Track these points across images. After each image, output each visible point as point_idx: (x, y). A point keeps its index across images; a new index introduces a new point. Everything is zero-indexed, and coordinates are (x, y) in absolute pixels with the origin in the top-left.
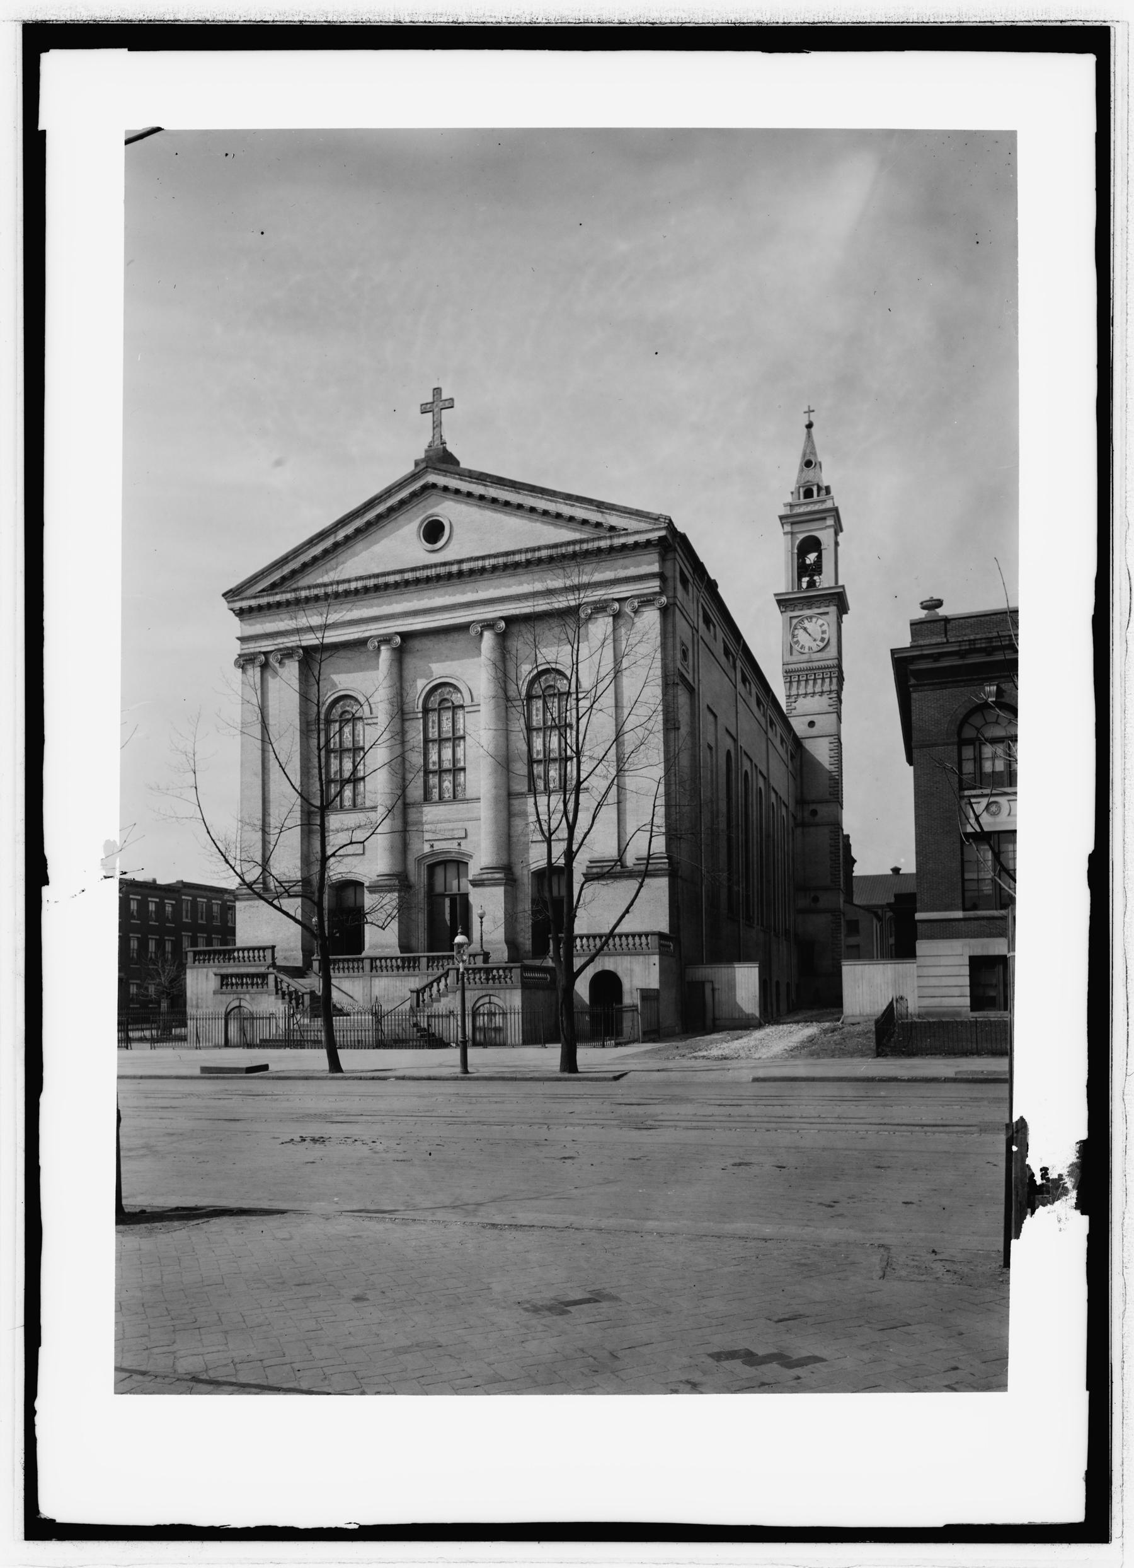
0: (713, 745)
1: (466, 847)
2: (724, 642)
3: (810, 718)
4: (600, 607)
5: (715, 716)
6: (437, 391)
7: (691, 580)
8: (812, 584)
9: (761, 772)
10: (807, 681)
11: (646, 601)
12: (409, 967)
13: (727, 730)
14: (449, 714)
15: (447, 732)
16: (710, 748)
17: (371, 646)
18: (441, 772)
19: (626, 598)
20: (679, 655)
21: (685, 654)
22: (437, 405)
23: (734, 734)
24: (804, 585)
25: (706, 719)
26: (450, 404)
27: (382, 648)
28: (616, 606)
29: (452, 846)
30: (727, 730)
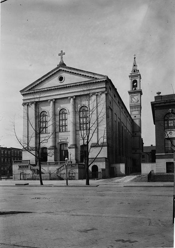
3: (135, 116)
4: (94, 94)
6: (62, 51)
8: (135, 89)
11: (103, 92)
19: (99, 92)
21: (110, 103)
22: (62, 54)
29: (65, 140)
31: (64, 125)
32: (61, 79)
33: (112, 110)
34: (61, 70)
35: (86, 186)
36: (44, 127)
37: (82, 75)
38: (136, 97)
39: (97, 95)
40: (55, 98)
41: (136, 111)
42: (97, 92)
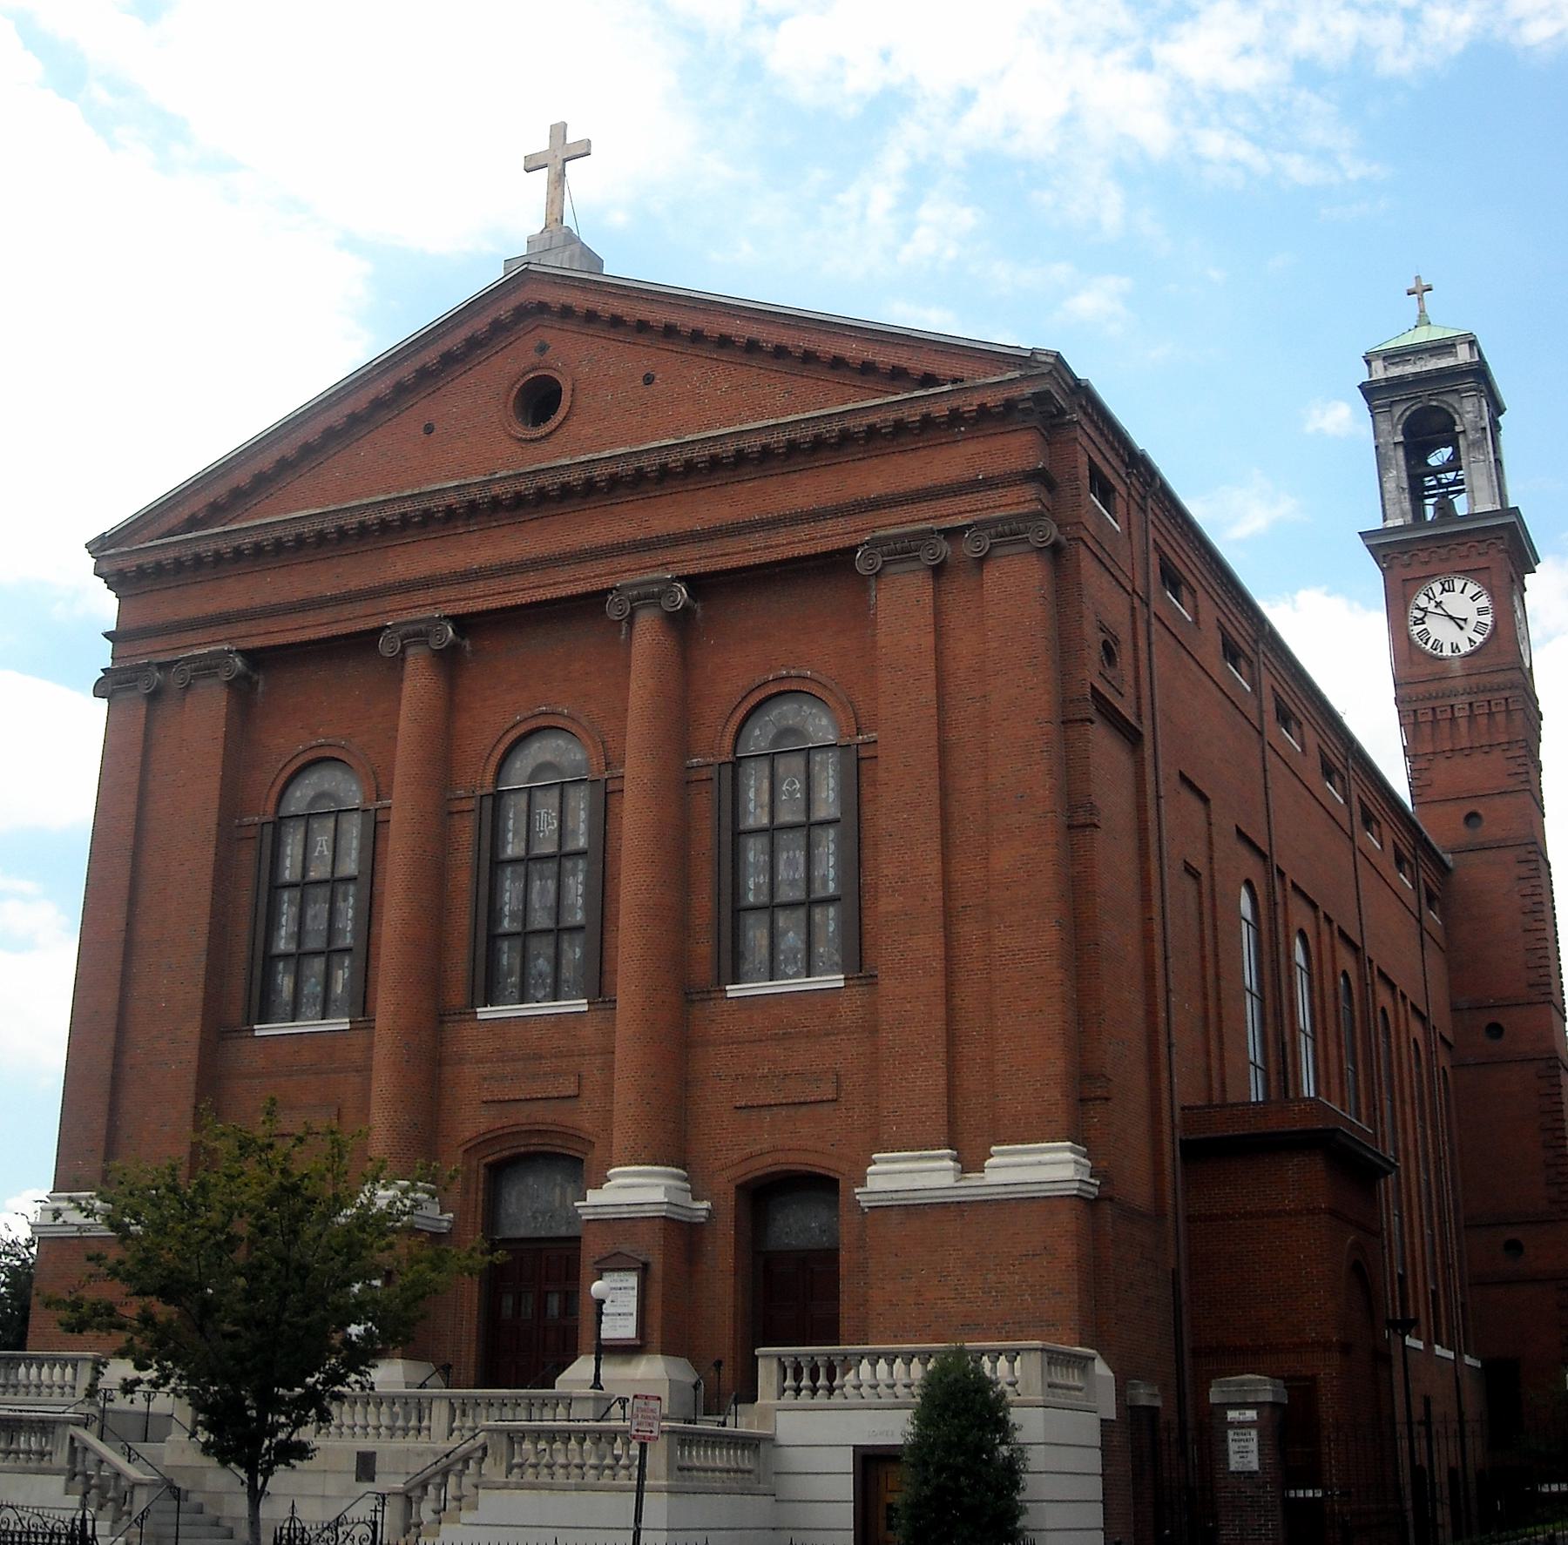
0: (1199, 863)
1: (584, 1119)
2: (1221, 627)
3: (1470, 807)
4: (902, 550)
5: (1204, 799)
6: (559, 131)
7: (1121, 488)
8: (1445, 508)
9: (1342, 933)
10: (1435, 722)
11: (1008, 533)
12: (814, 1391)
13: (1240, 834)
14: (553, 797)
15: (792, 883)
16: (1189, 870)
17: (385, 647)
18: (525, 935)
19: (960, 530)
20: (1095, 654)
21: (1109, 652)
22: (558, 157)
23: (1265, 849)
24: (1430, 513)
25: (1179, 811)
26: (583, 151)
27: (411, 651)
28: (945, 548)
29: (544, 1115)
30: (1240, 834)
31: (541, 920)
32: (540, 401)
33: (1131, 736)
34: (543, 307)
35: (1155, 1113)
36: (314, 942)
37: (556, 307)
38: (1456, 616)
39: (938, 571)
40: (257, 643)
41: (1497, 752)
42: (161, 666)
